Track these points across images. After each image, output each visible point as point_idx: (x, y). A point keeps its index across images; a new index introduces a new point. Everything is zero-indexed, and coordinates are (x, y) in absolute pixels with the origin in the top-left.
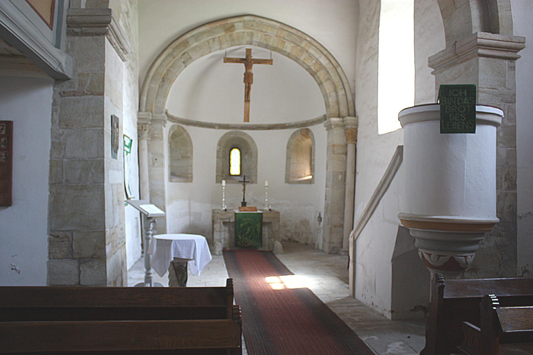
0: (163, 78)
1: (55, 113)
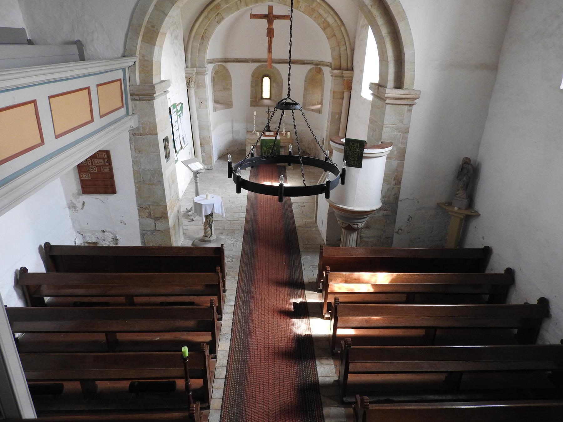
1: (131, 145)
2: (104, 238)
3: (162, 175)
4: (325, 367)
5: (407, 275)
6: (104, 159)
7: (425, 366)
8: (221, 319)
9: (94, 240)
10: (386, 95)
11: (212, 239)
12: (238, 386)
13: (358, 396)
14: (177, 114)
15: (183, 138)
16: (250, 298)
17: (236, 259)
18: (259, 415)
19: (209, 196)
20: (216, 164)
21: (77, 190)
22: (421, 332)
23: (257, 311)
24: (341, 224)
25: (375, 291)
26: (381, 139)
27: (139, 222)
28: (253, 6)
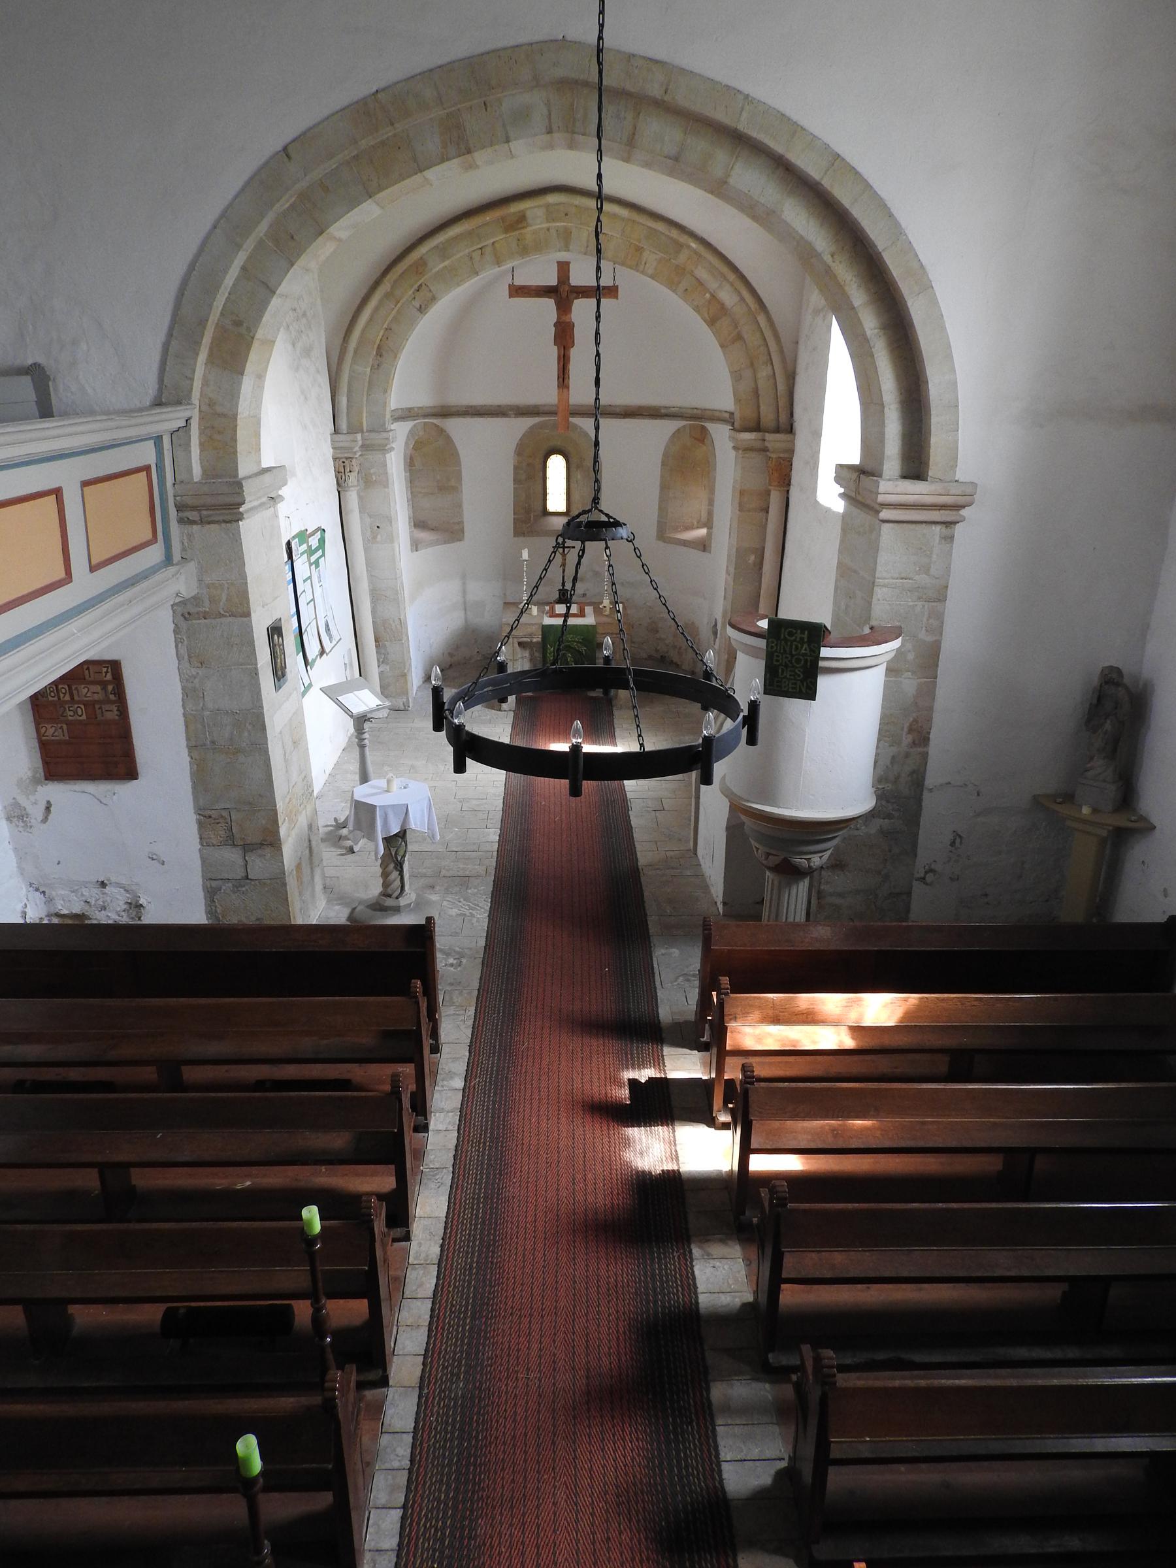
0: (379, 347)
1: (180, 645)
2: (103, 902)
3: (263, 728)
4: (718, 1264)
5: (948, 999)
6: (104, 684)
7: (1002, 1261)
8: (425, 1128)
9: (77, 909)
10: (881, 498)
11: (403, 902)
12: (468, 1321)
13: (806, 1349)
14: (309, 560)
15: (327, 625)
16: (508, 1068)
17: (471, 958)
18: (527, 1403)
19: (396, 784)
20: (419, 694)
21: (30, 769)
22: (992, 1164)
23: (528, 1106)
24: (763, 858)
25: (858, 1045)
26: (869, 618)
27: (202, 857)
28: (515, 263)
